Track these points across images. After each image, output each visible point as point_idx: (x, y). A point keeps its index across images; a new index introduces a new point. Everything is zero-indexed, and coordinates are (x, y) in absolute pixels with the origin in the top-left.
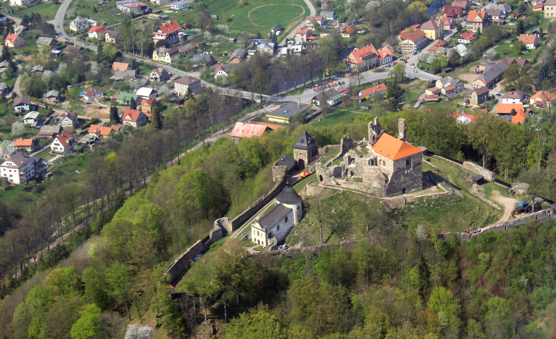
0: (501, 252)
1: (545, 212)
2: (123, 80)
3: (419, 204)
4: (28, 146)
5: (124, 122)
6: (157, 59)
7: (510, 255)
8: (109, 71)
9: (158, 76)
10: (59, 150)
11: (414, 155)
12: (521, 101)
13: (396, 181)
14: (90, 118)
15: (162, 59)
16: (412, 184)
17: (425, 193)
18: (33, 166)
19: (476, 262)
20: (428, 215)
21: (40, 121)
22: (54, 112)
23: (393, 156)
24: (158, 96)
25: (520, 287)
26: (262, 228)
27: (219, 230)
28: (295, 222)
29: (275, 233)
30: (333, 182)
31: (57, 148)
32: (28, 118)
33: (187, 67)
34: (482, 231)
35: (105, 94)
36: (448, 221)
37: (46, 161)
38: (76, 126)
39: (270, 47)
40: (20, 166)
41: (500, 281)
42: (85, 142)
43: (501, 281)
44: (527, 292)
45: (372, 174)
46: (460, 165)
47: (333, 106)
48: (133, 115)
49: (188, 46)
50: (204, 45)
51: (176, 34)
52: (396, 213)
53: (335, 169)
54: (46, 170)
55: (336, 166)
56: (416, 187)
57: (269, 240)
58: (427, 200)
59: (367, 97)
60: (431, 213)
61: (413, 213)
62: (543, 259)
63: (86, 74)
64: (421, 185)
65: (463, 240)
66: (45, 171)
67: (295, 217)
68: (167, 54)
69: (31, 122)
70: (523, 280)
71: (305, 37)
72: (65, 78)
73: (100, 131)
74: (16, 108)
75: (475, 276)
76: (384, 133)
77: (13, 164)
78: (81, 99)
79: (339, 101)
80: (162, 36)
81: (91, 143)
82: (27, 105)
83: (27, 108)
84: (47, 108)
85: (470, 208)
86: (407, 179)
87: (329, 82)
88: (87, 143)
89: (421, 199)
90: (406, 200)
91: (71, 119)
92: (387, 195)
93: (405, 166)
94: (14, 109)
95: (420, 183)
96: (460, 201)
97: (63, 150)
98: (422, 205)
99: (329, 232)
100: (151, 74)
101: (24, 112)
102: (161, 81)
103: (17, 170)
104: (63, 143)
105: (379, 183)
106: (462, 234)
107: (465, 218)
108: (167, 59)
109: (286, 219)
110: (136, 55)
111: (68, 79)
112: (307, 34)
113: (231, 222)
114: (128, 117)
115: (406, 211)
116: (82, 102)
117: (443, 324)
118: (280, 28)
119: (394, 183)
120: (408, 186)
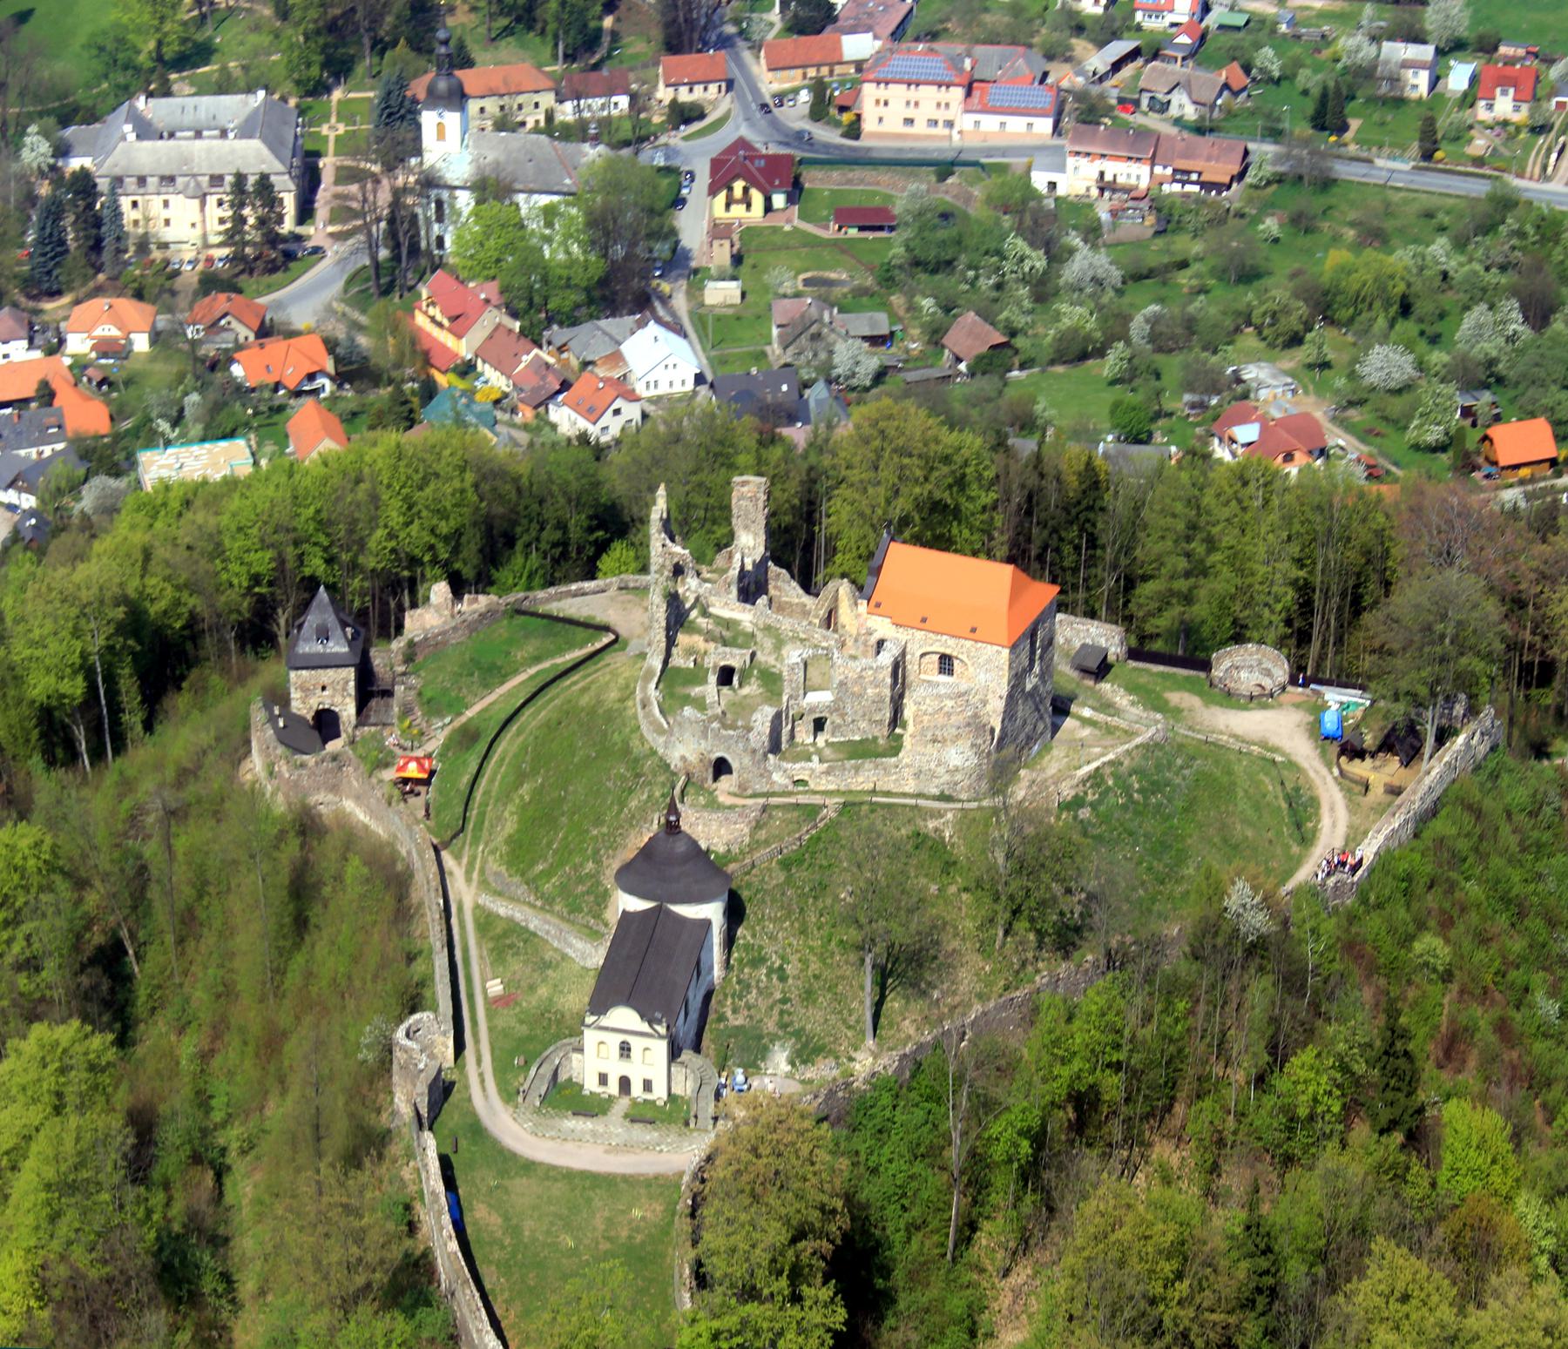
12: (32, 345)
45: (949, 715)
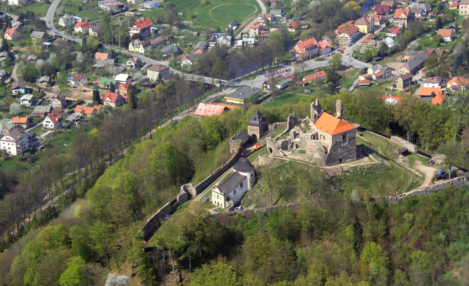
0: (422, 212)
1: (460, 179)
2: (103, 68)
3: (353, 173)
4: (24, 123)
5: (105, 103)
6: (132, 50)
7: (430, 215)
8: (92, 60)
9: (133, 64)
10: (50, 126)
11: (349, 131)
12: (440, 85)
13: (334, 153)
14: (76, 100)
15: (137, 50)
16: (348, 155)
17: (359, 163)
18: (28, 140)
19: (402, 221)
20: (361, 182)
21: (34, 102)
22: (45, 94)
23: (332, 132)
24: (133, 81)
25: (439, 242)
26: (221, 192)
27: (185, 194)
28: (249, 187)
29: (232, 197)
30: (281, 154)
31: (48, 125)
32: (24, 100)
33: (157, 56)
34: (406, 195)
35: (88, 80)
36: (378, 186)
37: (39, 136)
38: (64, 106)
39: (227, 39)
40: (17, 140)
41: (422, 237)
42: (71, 120)
43: (423, 237)
44: (445, 246)
45: (314, 146)
46: (388, 139)
47: (281, 89)
48: (112, 97)
49: (159, 39)
50: (172, 38)
51: (148, 28)
52: (334, 180)
53: (283, 142)
54: (38, 143)
55: (284, 140)
56: (351, 158)
57: (227, 203)
58: (360, 169)
59: (310, 82)
60: (363, 180)
61: (348, 180)
62: (458, 219)
63: (73, 63)
64: (355, 156)
65: (390, 202)
66: (38, 145)
67: (248, 183)
68: (141, 45)
69: (26, 103)
70: (441, 236)
71: (257, 31)
72: (55, 66)
73: (84, 111)
74: (14, 91)
75: (401, 233)
76: (324, 113)
77: (11, 138)
78: (68, 84)
79: (286, 85)
80: (137, 30)
81: (77, 121)
82: (22, 88)
83: (22, 91)
84: (39, 91)
85: (396, 176)
86: (343, 151)
87: (278, 69)
88: (74, 121)
89: (355, 168)
90: (342, 169)
91: (60, 101)
92: (326, 165)
93: (342, 140)
94: (12, 92)
95: (355, 154)
96: (388, 169)
97: (53, 127)
98: (356, 173)
99: (278, 195)
100: (128, 63)
101: (20, 95)
102: (136, 68)
103: (15, 143)
104: (54, 121)
105: (320, 154)
106: (390, 197)
107: (392, 184)
108: (141, 50)
109: (242, 185)
110: (115, 47)
111: (57, 67)
112: (259, 29)
113: (195, 187)
114: (108, 99)
115: (343, 178)
116: (70, 86)
117: (373, 273)
118: (236, 24)
119: (333, 154)
120: (344, 157)
